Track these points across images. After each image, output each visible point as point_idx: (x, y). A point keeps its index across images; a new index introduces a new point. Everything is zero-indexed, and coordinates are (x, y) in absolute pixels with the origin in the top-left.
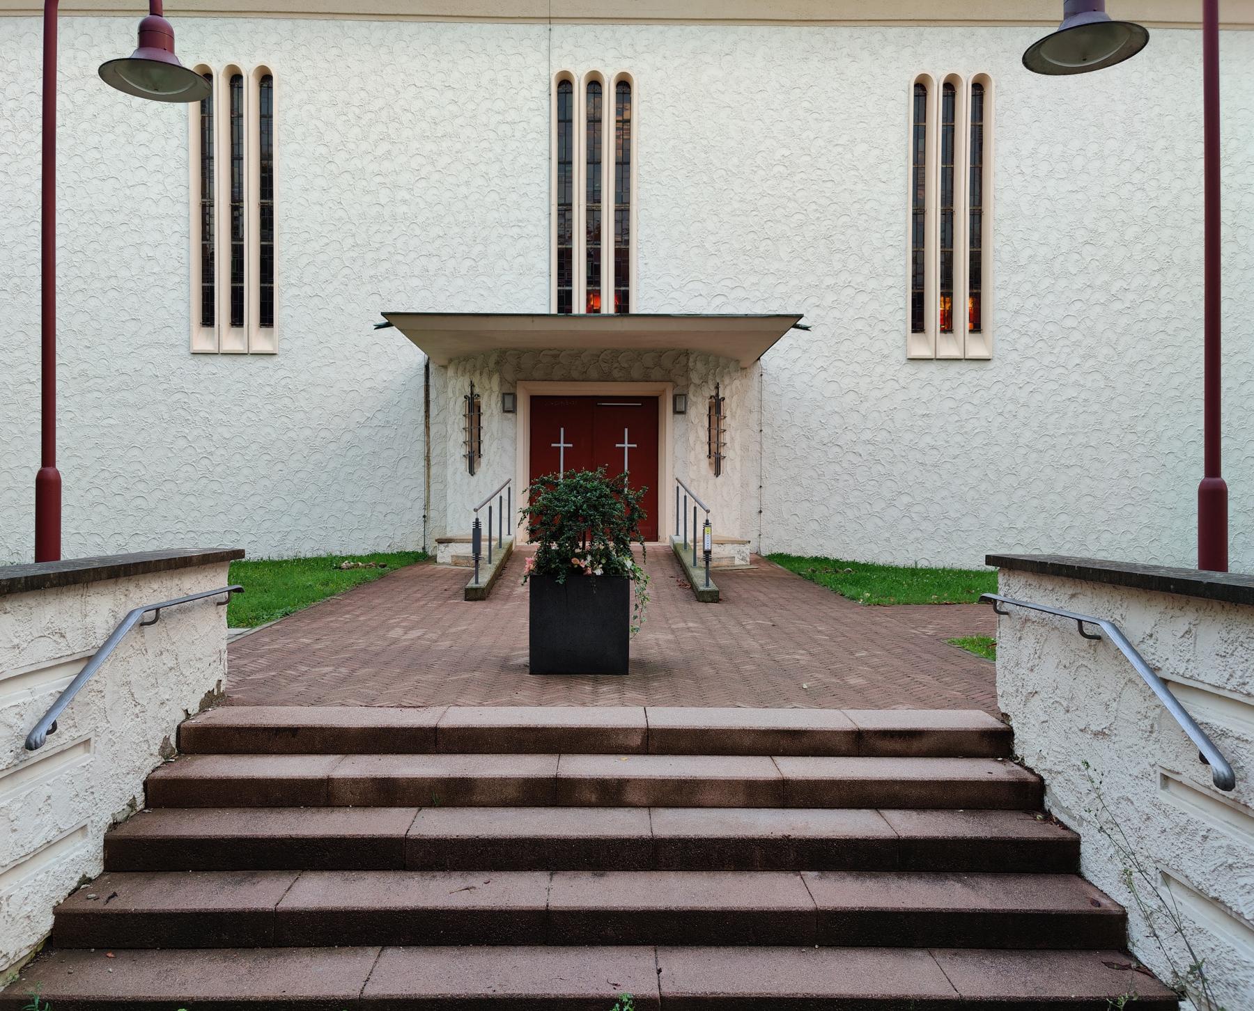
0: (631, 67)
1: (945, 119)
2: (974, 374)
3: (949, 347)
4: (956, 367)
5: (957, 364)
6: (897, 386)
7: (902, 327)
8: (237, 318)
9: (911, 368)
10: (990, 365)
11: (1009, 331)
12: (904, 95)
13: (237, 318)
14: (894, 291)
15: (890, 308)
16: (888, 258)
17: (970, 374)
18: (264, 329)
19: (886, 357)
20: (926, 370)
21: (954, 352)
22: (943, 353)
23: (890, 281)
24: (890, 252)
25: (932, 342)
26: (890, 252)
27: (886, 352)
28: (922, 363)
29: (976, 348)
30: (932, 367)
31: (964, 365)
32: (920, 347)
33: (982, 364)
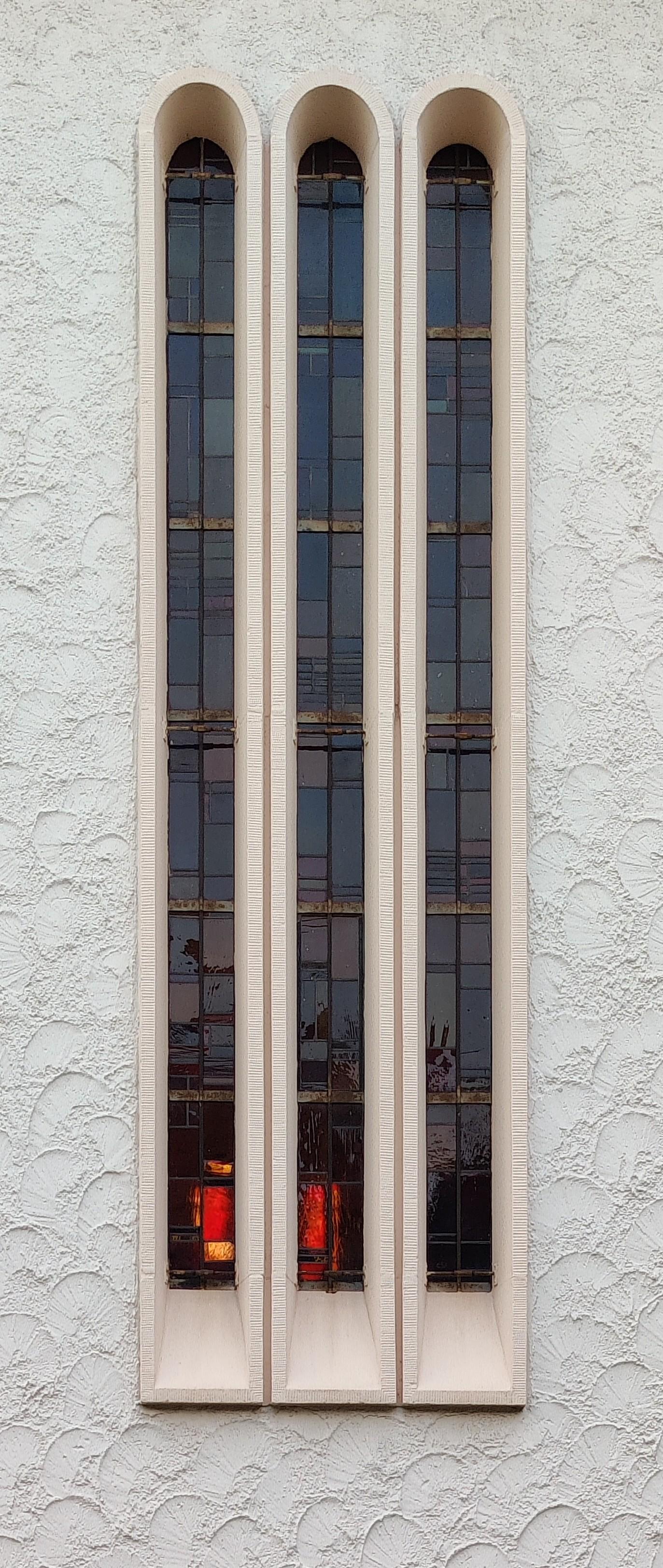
0: (198, 65)
1: (306, 306)
2: (446, 1474)
3: (336, 1350)
4: (363, 1441)
5: (372, 1425)
6: (95, 1530)
7: (118, 1258)
8: (333, 1257)
9: (160, 1448)
10: (522, 1435)
11: (601, 1278)
12: (113, 185)
13: (333, 1257)
14: (75, 1092)
15: (66, 1173)
16: (50, 941)
17: (432, 1470)
18: (319, 1297)
19: (39, 1394)
20: (230, 1456)
21: (233, 1379)
22: (303, 1381)
23: (56, 1049)
24: (57, 914)
25: (267, 1332)
26: (57, 914)
27: (45, 1376)
28: (207, 1423)
29: (465, 1350)
30: (256, 1440)
31: (399, 1431)
32: (209, 1350)
33: (510, 1419)
